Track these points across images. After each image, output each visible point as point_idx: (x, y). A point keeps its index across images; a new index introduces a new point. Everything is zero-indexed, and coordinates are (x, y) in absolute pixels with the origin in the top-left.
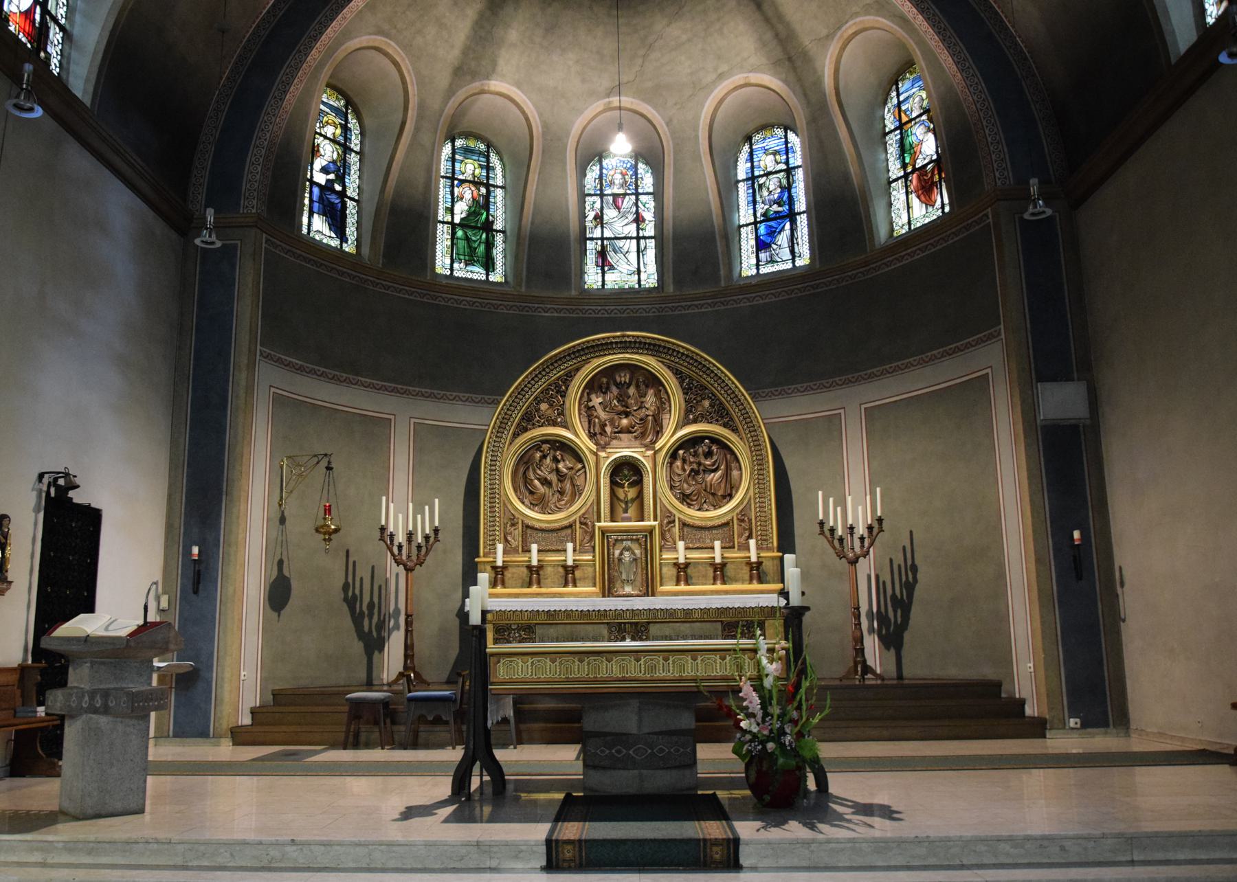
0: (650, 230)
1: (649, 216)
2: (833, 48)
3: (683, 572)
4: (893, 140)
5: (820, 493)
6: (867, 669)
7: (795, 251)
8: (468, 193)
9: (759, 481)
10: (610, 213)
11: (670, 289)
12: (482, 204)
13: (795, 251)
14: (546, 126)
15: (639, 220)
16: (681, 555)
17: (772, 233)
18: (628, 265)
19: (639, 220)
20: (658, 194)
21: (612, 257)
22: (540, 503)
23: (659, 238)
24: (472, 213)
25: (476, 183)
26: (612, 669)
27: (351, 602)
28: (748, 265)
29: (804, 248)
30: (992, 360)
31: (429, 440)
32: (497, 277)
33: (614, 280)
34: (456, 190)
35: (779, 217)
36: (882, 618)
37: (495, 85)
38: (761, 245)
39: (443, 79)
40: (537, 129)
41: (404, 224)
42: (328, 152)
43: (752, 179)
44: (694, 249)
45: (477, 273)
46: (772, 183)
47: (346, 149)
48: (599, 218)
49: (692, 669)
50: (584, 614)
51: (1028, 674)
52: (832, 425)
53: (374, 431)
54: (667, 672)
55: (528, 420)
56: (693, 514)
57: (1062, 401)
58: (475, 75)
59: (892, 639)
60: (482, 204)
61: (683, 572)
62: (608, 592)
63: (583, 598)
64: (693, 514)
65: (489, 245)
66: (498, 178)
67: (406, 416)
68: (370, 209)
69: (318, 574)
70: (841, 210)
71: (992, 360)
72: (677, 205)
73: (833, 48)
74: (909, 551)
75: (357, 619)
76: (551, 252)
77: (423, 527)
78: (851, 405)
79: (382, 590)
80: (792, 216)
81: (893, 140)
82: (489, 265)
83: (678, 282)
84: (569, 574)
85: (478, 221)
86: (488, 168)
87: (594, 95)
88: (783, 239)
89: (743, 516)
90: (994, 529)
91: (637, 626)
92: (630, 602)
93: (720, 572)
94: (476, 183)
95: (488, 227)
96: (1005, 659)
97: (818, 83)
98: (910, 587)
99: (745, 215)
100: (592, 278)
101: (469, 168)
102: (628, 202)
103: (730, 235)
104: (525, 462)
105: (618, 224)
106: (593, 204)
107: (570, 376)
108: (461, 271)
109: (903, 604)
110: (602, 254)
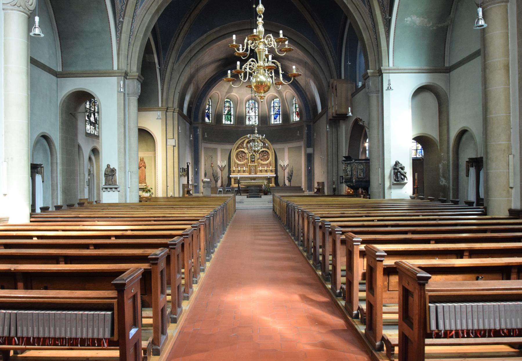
0: (257, 114)
1: (257, 112)
2: (285, 92)
3: (261, 171)
4: (294, 105)
5: (350, 108)
6: (285, 185)
7: (279, 121)
8: (227, 109)
9: (272, 158)
10: (250, 111)
11: (260, 125)
12: (229, 111)
13: (279, 121)
14: (240, 99)
15: (255, 112)
16: (261, 168)
17: (277, 117)
18: (252, 120)
19: (255, 112)
20: (258, 108)
21: (251, 119)
22: (240, 160)
23: (258, 115)
24: (228, 112)
25: (228, 107)
26: (252, 183)
27: (213, 175)
28: (273, 122)
29: (281, 120)
30: (302, 144)
31: (223, 150)
32: (232, 123)
33: (251, 123)
34: (262, 204)
35: (277, 114)
36: (289, 178)
37: (232, 94)
38: (275, 119)
39: (225, 94)
40: (239, 100)
41: (218, 117)
42: (207, 106)
43: (274, 107)
44: (264, 119)
45: (229, 122)
46: (277, 108)
47: (209, 105)
48: (249, 112)
49: (259, 183)
50: (247, 177)
51: (303, 186)
52: (283, 149)
53: (215, 150)
54: (257, 184)
55: (238, 148)
56: (263, 162)
57: (310, 150)
58: (229, 93)
59: (290, 181)
60: (229, 111)
61: (261, 171)
62: (250, 174)
63: (246, 175)
64: (263, 162)
65: (231, 118)
66: (232, 106)
67: (220, 147)
68: (213, 115)
69: (210, 173)
70: (286, 117)
71: (302, 144)
72: (261, 111)
73: (285, 92)
74: (292, 168)
75: (214, 178)
76: (240, 119)
77: (223, 166)
78: (286, 146)
79: (217, 174)
80: (279, 114)
81: (294, 105)
82: (231, 121)
83: (261, 124)
84: (244, 171)
85: (229, 114)
86: (230, 104)
87: (248, 94)
88: (278, 118)
89: (270, 162)
90: (301, 167)
91: (254, 179)
92: (253, 175)
93: (266, 171)
94: (228, 107)
95: (230, 115)
96: (301, 184)
97: (283, 96)
98: (292, 174)
99: (272, 113)
100: (247, 123)
101: (227, 104)
102: (253, 109)
103: (269, 117)
104: (237, 154)
105: (252, 114)
106: (248, 109)
107: (244, 141)
108: (226, 123)
109: (291, 176)
110: (249, 118)
